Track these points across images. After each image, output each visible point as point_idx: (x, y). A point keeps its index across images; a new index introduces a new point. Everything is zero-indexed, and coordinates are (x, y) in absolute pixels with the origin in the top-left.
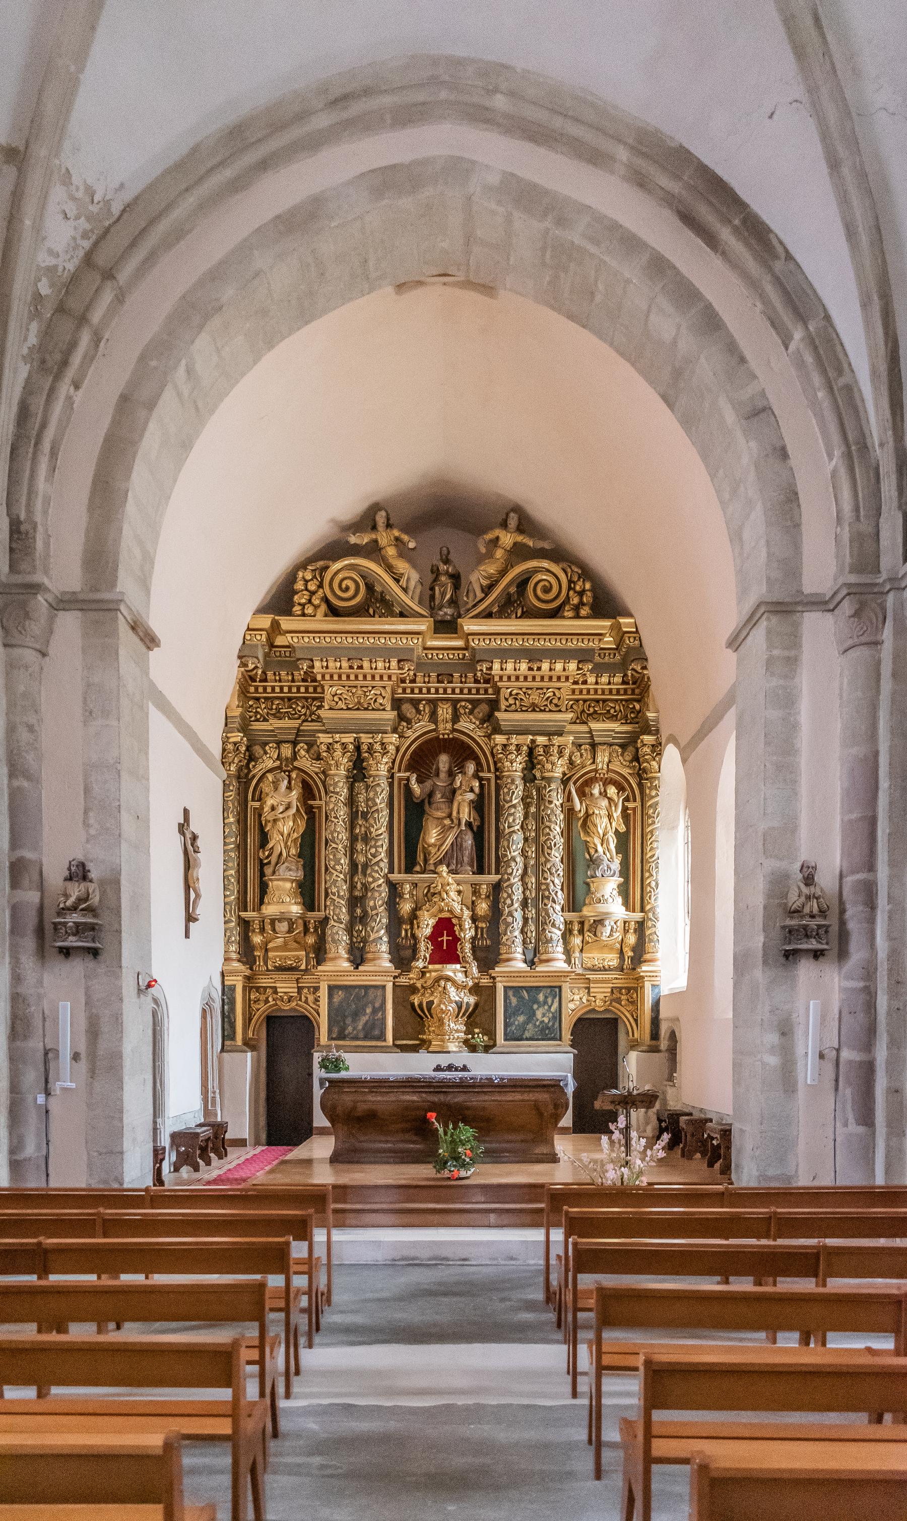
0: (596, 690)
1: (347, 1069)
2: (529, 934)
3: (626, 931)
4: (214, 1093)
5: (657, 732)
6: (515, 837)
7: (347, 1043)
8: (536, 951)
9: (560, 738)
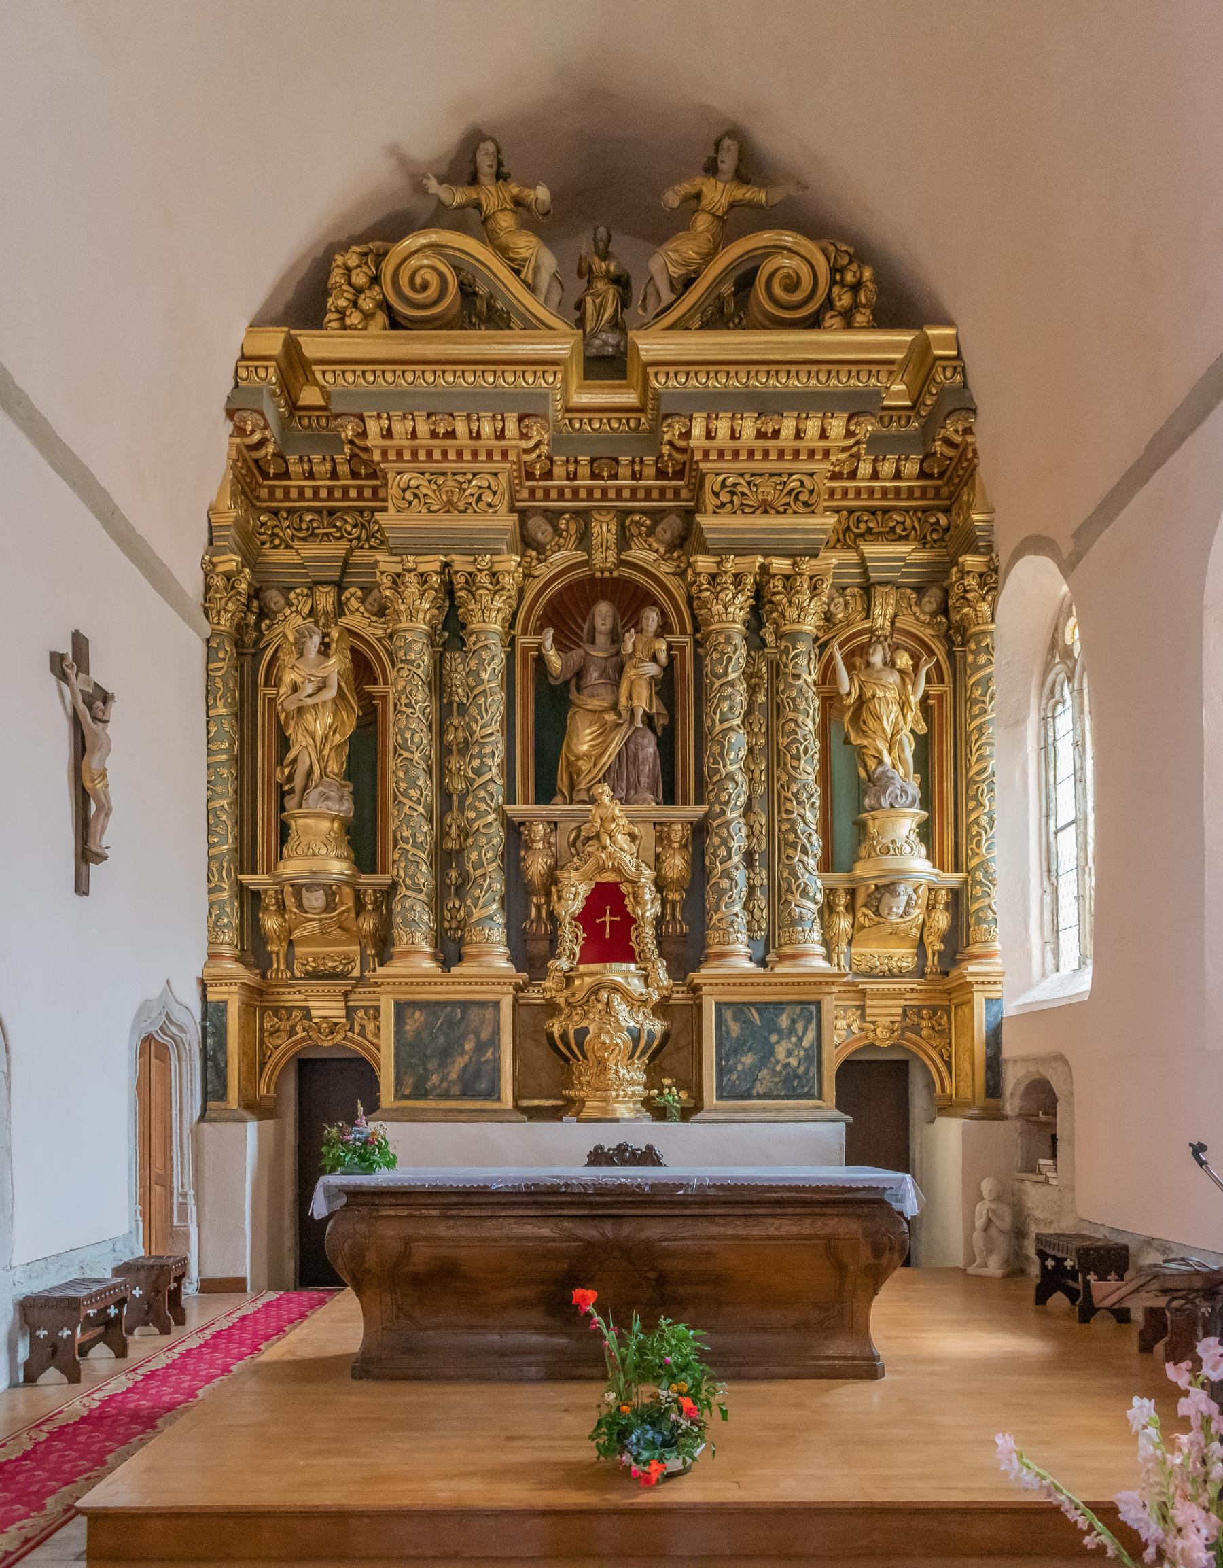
0: (871, 491)
1: (391, 1163)
2: (757, 913)
3: (930, 908)
4: (184, 1195)
5: (990, 548)
6: (733, 738)
7: (431, 1104)
8: (768, 943)
9: (813, 562)
